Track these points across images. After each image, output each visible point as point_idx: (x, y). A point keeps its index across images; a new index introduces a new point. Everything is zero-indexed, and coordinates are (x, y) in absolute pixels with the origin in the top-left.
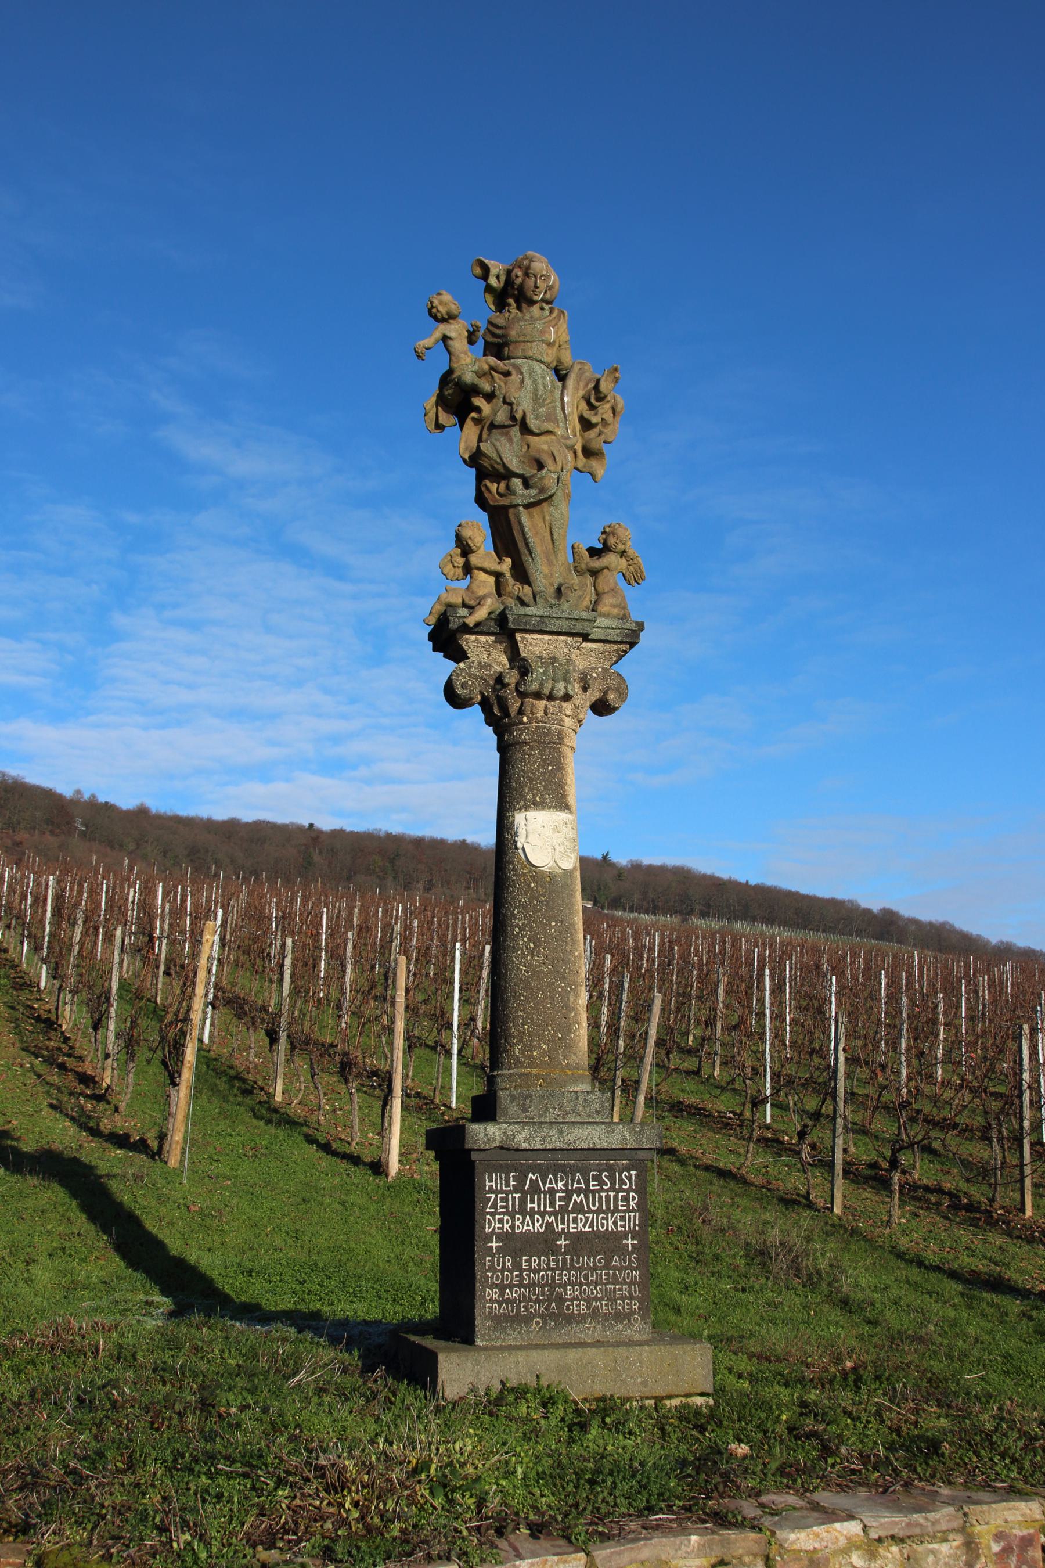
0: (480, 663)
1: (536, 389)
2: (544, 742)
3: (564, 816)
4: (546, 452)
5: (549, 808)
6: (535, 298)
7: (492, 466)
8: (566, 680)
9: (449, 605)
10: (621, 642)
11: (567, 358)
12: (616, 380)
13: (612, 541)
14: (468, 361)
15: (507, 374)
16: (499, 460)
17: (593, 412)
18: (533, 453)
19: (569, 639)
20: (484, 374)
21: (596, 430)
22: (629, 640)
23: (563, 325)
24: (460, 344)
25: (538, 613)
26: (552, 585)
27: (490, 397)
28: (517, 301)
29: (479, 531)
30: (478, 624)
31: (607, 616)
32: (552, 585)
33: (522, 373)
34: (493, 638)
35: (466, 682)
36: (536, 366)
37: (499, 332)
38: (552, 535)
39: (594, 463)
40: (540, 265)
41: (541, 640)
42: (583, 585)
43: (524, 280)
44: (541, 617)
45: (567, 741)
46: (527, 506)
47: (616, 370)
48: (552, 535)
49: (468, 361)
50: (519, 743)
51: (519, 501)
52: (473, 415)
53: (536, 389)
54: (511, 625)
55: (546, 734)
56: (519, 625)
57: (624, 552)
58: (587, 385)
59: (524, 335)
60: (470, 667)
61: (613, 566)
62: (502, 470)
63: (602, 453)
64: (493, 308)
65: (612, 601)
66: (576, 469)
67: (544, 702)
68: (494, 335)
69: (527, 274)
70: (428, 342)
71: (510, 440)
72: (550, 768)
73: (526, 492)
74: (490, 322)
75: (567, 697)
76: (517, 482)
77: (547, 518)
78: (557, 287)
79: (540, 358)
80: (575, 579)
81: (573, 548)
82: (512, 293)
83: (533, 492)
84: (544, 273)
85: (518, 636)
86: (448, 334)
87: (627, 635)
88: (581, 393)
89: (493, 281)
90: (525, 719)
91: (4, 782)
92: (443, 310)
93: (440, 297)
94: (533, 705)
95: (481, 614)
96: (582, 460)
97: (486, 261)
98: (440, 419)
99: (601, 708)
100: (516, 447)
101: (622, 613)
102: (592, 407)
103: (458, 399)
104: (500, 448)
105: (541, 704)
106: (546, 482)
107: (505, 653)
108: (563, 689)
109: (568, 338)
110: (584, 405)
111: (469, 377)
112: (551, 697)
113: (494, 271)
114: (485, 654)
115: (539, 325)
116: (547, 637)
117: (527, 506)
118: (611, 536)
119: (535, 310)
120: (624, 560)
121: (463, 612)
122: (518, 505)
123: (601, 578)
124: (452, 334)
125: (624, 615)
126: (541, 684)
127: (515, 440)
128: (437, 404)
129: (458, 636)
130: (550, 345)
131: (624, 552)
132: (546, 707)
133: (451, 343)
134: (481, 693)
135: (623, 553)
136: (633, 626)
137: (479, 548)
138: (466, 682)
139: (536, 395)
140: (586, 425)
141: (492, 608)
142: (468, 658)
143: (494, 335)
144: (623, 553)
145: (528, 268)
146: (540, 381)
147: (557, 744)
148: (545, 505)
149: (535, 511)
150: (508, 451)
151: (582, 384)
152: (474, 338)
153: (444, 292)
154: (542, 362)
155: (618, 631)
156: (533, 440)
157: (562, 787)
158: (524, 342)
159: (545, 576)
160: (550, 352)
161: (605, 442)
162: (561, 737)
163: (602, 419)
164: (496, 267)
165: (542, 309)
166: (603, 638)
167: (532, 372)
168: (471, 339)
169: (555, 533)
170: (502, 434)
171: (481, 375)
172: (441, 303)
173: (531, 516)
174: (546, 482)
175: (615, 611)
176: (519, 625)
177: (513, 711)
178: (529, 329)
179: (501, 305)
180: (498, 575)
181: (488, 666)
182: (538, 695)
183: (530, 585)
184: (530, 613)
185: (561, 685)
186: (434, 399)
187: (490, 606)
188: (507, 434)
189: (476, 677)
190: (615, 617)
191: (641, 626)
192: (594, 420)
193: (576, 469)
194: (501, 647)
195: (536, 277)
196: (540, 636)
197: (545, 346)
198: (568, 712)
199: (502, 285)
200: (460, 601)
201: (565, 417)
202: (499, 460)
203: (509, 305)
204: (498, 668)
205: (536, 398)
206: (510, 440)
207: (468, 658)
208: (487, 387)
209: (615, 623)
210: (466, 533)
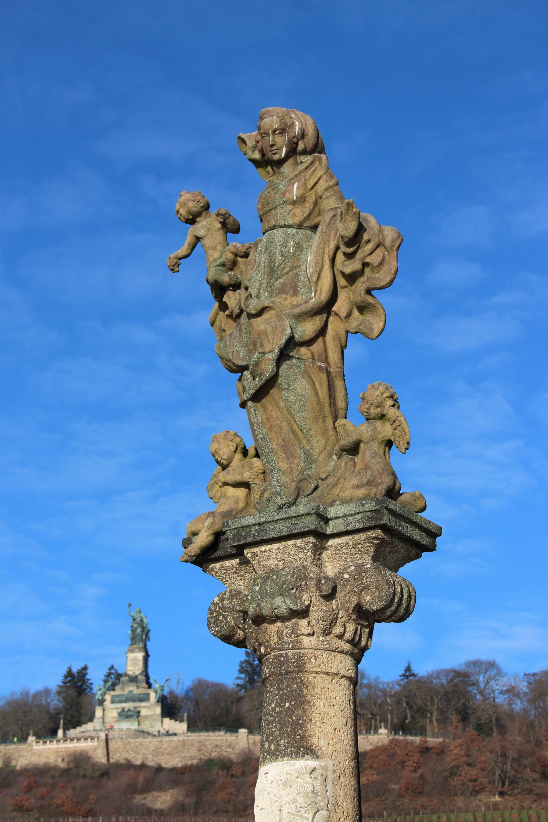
1: (271, 262)
3: (309, 763)
5: (283, 757)
19: (299, 542)
22: (372, 524)
34: (237, 560)
41: (270, 551)
44: (259, 524)
45: (312, 665)
53: (271, 262)
55: (283, 663)
61: (365, 437)
72: (287, 705)
79: (283, 223)
84: (276, 126)
87: (370, 519)
91: (348, 806)
105: (272, 628)
116: (275, 546)
130: (294, 203)
147: (297, 672)
148: (274, 392)
154: (289, 226)
155: (359, 516)
157: (303, 726)
159: (285, 473)
162: (300, 663)
166: (343, 529)
176: (239, 540)
197: (289, 207)
209: (350, 509)
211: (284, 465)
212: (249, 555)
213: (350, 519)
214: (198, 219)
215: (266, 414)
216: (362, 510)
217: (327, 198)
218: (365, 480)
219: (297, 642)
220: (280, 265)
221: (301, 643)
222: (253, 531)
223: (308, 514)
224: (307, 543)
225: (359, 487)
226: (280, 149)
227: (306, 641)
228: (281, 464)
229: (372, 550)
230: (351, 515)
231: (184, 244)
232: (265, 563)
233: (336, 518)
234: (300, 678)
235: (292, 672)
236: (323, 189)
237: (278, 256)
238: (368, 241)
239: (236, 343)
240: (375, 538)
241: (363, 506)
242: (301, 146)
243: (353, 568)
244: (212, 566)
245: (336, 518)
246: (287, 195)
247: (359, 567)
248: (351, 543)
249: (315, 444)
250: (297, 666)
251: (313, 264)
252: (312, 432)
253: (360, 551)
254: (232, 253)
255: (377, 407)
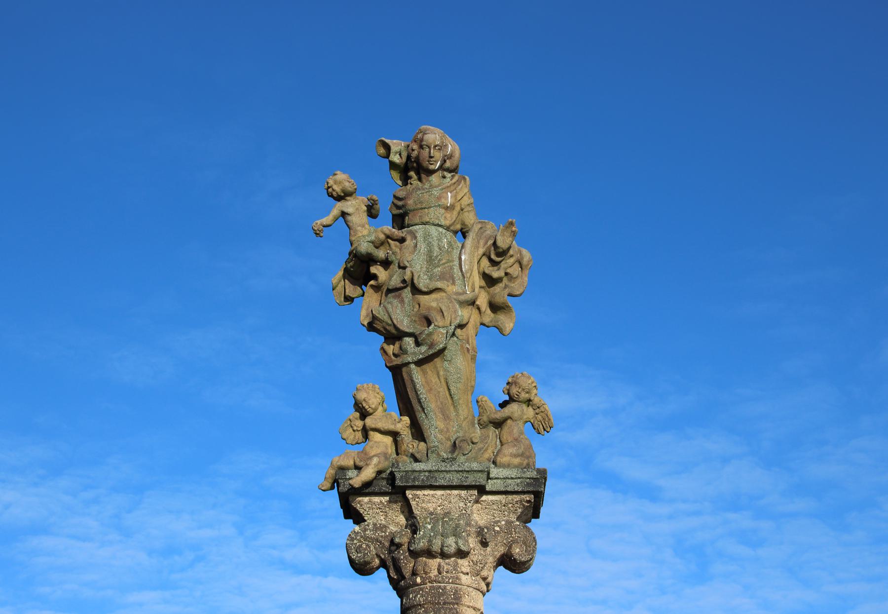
0: (375, 525)
1: (430, 251)
2: (439, 603)
4: (435, 309)
6: (432, 167)
7: (385, 329)
8: (456, 534)
9: (342, 469)
10: (523, 493)
11: (470, 218)
12: (514, 234)
13: (514, 390)
14: (365, 232)
15: (402, 240)
16: (390, 322)
17: (496, 268)
18: (424, 312)
19: (463, 493)
20: (382, 244)
21: (501, 285)
22: (531, 489)
23: (464, 189)
24: (359, 218)
25: (426, 469)
26: (448, 439)
27: (386, 264)
28: (418, 174)
29: (379, 394)
30: (367, 484)
31: (508, 466)
32: (448, 439)
33: (416, 238)
34: (387, 498)
35: (360, 546)
36: (433, 230)
37: (400, 203)
38: (449, 390)
39: (502, 317)
40: (434, 136)
41: (433, 496)
42: (484, 438)
43: (419, 152)
44: (430, 471)
45: (466, 600)
46: (420, 363)
47: (512, 224)
48: (449, 390)
49: (365, 232)
50: (414, 606)
51: (410, 359)
52: (372, 282)
53: (430, 251)
54: (398, 483)
56: (407, 482)
57: (530, 400)
58: (486, 243)
59: (421, 203)
60: (365, 530)
61: (516, 415)
62: (394, 331)
63: (508, 307)
64: (400, 183)
65: (513, 450)
66: (482, 324)
67: (438, 560)
68: (398, 207)
69: (421, 147)
70: (327, 220)
71: (402, 302)
73: (417, 349)
74: (395, 197)
75: (462, 554)
76: (409, 341)
77: (441, 373)
78: (457, 154)
80: (477, 432)
81: (477, 402)
82: (413, 168)
83: (423, 349)
84: (438, 143)
85: (409, 494)
86: (346, 210)
88: (481, 251)
89: (396, 159)
90: (419, 580)
92: (337, 189)
93: (335, 177)
94: (426, 564)
95: (368, 473)
96: (489, 316)
97: (387, 141)
98: (347, 291)
99: (512, 564)
100: (408, 308)
101: (525, 463)
102: (494, 263)
103: (360, 270)
104: (390, 310)
105: (434, 563)
106: (435, 337)
107: (403, 512)
108: (454, 545)
109: (472, 201)
110: (485, 262)
111: (364, 247)
112: (444, 555)
113: (394, 149)
114: (380, 512)
115: (436, 192)
116: (439, 493)
117: (420, 363)
118: (513, 386)
119: (435, 179)
120: (530, 409)
121: (351, 473)
122: (409, 363)
123: (506, 429)
124: (349, 210)
125: (528, 464)
126: (430, 541)
127: (406, 300)
128: (344, 277)
129: (351, 499)
130: (447, 208)
131: (530, 400)
132: (439, 565)
133: (349, 218)
134: (378, 556)
135: (529, 402)
136: (534, 474)
137: (375, 410)
138: (360, 546)
139: (431, 257)
140: (490, 281)
141: (381, 467)
142: (365, 521)
143: (398, 207)
144: (529, 402)
145: (422, 140)
146: (435, 244)
147: (453, 604)
148: (437, 361)
149: (427, 367)
150: (401, 315)
151: (482, 242)
152: (373, 211)
153: (338, 172)
155: (519, 481)
156: (423, 299)
158: (422, 209)
159: (441, 431)
160: (448, 215)
161: (510, 295)
162: (457, 598)
163: (506, 274)
164: (397, 145)
165: (444, 177)
166: (502, 489)
167: (427, 236)
168: (372, 212)
169: (452, 388)
170: (395, 297)
171: (378, 245)
172: (335, 182)
173: (425, 373)
174: (435, 337)
175: (517, 461)
176: (407, 482)
177: (407, 573)
178: (426, 196)
179: (406, 180)
180: (395, 435)
181: (383, 528)
182: (429, 553)
183: (425, 442)
184: (418, 469)
185: (451, 541)
186: (341, 273)
187: (376, 465)
188: (399, 296)
189: (372, 540)
190: (516, 467)
191: (543, 475)
192: (496, 274)
193: (482, 324)
194: (397, 507)
195: (429, 148)
196: (432, 492)
197: (443, 211)
198: (464, 570)
199: (404, 160)
200: (352, 463)
201: (463, 275)
202: (390, 322)
203: (411, 178)
204: (393, 528)
205: (430, 259)
206: (402, 302)
207: (365, 521)
208: (381, 254)
209: (513, 473)
210: (361, 396)
211: (441, 425)
212: (410, 496)
213: (510, 481)
214: (348, 198)
215: (426, 378)
216: (523, 476)
217: (468, 211)
218: (520, 451)
219: (457, 578)
220: (437, 257)
221: (460, 579)
222: (422, 476)
223: (481, 471)
224: (471, 496)
225: (516, 456)
226: (436, 162)
227: (464, 579)
228: (438, 423)
229: (520, 510)
230: (512, 478)
231: (328, 214)
232: (423, 505)
233: (496, 478)
234: (456, 609)
235: (450, 603)
236: (466, 203)
237: (436, 249)
238: (512, 256)
239: (398, 312)
240: (528, 502)
241: (524, 473)
242: (448, 164)
243: (503, 523)
244: (360, 499)
245: (496, 478)
246: (443, 200)
247: (509, 523)
248: (503, 502)
249: (460, 412)
250: (454, 599)
251: (467, 262)
252: (461, 402)
253: (509, 509)
254: (385, 234)
255: (527, 393)
